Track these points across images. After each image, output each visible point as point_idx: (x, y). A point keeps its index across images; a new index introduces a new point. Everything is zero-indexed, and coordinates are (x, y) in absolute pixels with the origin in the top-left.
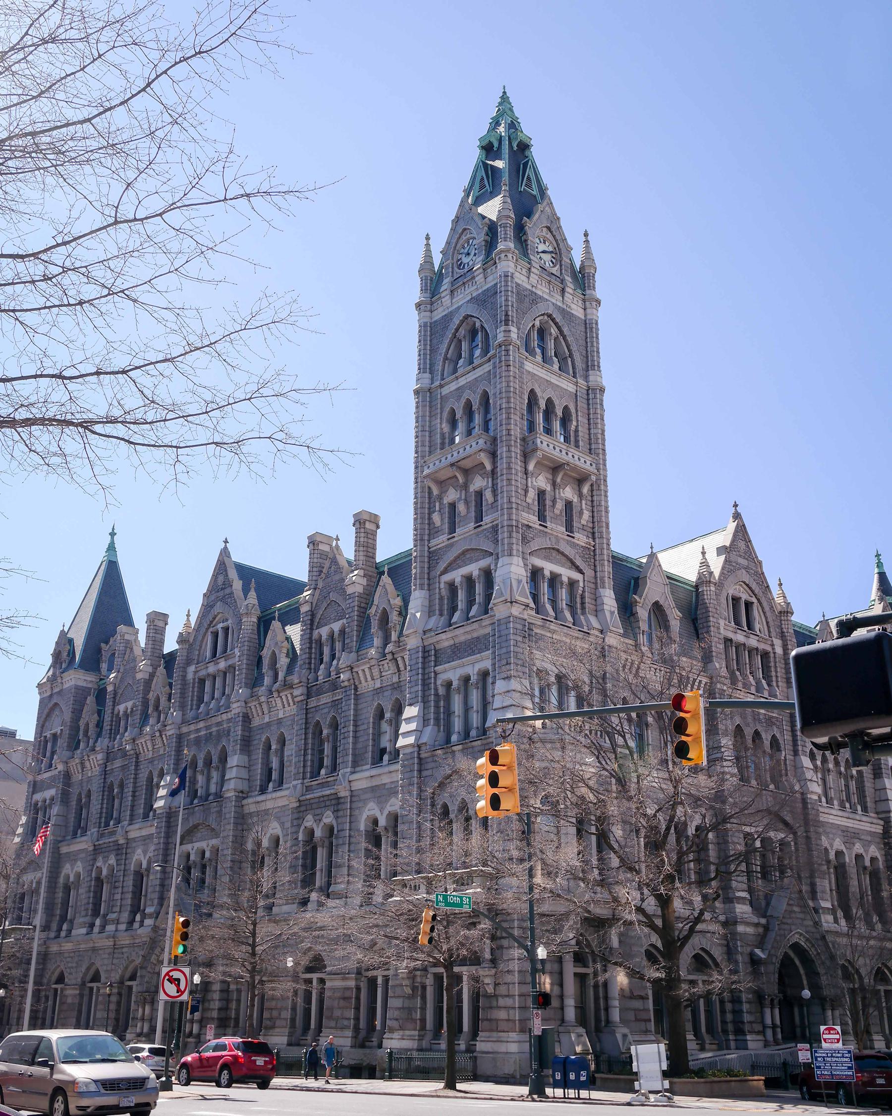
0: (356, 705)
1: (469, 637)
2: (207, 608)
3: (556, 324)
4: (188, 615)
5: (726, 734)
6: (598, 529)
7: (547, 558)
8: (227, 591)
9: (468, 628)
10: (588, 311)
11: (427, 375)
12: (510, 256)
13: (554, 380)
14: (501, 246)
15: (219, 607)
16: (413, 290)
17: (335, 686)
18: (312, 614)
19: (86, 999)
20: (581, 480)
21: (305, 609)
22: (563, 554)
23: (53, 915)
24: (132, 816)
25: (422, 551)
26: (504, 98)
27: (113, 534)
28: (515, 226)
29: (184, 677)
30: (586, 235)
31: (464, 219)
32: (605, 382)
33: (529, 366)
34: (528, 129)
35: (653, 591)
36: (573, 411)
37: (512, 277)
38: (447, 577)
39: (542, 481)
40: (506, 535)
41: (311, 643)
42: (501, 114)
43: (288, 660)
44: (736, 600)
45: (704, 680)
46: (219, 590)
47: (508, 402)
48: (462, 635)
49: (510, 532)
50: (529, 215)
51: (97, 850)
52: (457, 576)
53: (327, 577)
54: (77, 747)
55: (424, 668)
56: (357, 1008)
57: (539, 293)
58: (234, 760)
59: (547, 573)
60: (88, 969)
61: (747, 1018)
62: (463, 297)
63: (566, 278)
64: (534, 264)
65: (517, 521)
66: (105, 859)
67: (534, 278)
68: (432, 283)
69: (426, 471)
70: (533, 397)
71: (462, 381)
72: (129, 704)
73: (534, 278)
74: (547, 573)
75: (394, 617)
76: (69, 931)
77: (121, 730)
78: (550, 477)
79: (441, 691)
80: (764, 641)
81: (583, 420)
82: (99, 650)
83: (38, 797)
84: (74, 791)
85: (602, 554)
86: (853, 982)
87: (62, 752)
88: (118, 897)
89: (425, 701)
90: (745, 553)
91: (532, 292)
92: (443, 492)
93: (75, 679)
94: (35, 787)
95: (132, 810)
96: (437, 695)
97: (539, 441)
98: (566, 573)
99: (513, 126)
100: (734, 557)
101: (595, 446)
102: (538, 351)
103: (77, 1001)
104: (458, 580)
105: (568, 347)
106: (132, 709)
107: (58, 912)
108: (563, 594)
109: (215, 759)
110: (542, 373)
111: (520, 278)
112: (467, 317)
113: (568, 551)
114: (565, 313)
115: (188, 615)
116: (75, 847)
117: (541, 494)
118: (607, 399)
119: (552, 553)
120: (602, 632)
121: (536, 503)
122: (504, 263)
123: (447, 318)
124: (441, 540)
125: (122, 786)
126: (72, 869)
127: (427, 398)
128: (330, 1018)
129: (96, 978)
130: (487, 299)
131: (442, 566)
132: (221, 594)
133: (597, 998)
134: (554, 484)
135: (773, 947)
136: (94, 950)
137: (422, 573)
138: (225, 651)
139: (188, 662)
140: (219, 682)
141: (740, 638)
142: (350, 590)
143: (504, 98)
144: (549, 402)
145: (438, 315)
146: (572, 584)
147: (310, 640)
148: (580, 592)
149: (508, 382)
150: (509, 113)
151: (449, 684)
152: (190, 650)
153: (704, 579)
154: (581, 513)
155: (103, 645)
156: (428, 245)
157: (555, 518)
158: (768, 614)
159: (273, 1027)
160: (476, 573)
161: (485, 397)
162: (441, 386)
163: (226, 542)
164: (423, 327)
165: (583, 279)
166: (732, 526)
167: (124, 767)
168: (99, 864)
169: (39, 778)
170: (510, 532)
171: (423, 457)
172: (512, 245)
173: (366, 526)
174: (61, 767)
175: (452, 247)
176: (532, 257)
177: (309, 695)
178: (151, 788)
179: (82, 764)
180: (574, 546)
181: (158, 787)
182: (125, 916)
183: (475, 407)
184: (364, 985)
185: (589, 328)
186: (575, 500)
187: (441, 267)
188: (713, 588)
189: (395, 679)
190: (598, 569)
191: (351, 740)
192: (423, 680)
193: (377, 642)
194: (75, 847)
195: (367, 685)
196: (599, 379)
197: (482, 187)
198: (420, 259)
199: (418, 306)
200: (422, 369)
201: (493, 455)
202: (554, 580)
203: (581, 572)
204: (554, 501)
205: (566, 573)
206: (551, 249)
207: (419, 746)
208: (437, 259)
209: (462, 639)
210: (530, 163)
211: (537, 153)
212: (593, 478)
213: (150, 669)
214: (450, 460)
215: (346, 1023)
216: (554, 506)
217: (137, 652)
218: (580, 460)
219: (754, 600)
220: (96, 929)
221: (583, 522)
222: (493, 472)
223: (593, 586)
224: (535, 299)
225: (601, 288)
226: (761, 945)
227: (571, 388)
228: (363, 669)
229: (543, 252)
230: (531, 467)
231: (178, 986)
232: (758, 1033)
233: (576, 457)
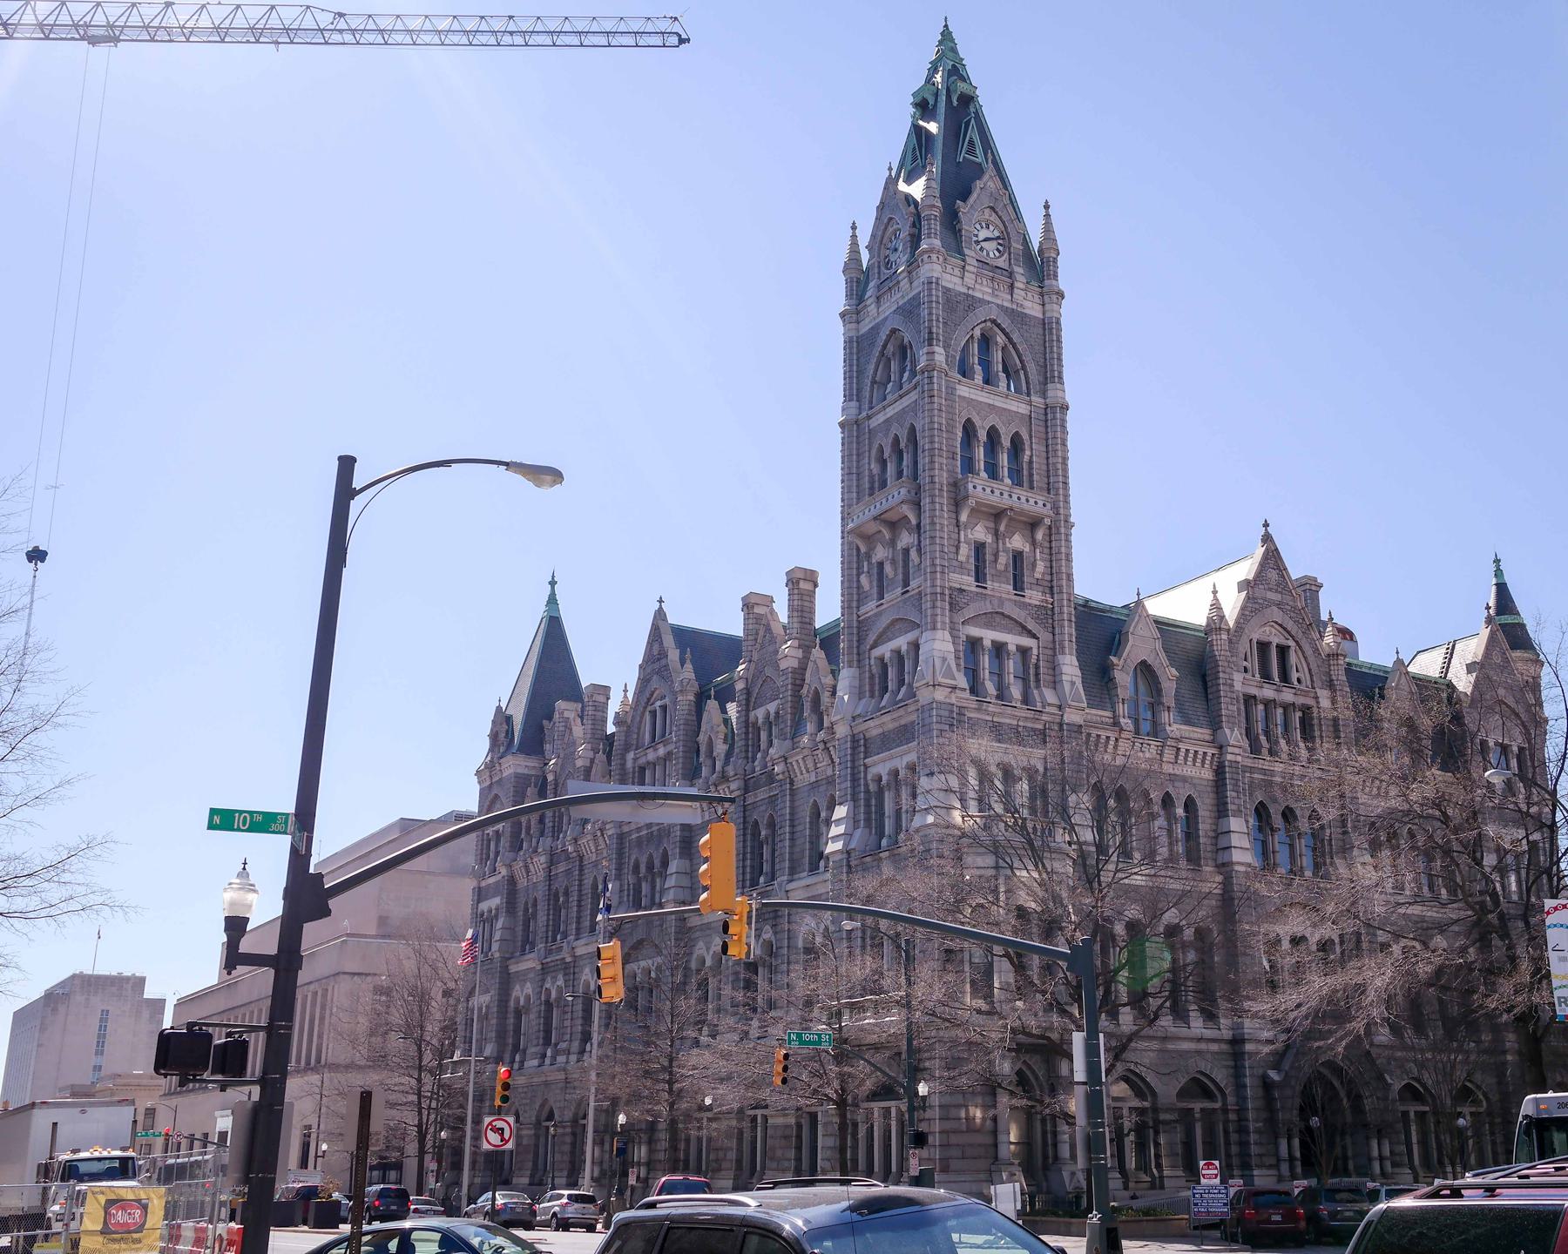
0: (792, 801)
1: (896, 724)
2: (644, 682)
3: (1003, 330)
4: (626, 691)
5: (1238, 813)
6: (1057, 577)
7: (989, 625)
8: (663, 662)
9: (895, 715)
10: (1048, 307)
11: (854, 404)
12: (934, 257)
13: (999, 402)
15: (655, 682)
16: (836, 296)
17: (770, 778)
18: (748, 691)
19: (542, 1140)
20: (1033, 524)
21: (740, 686)
22: (1009, 617)
23: (506, 1045)
24: (578, 929)
25: (850, 621)
26: (946, 35)
27: (553, 583)
28: (943, 215)
29: (623, 765)
30: (1047, 207)
31: (891, 201)
33: (963, 391)
35: (1140, 646)
36: (1025, 436)
38: (876, 652)
39: (980, 533)
40: (929, 605)
41: (747, 727)
43: (726, 747)
44: (1263, 647)
45: (1210, 751)
46: (654, 665)
47: (932, 442)
48: (888, 722)
49: (934, 601)
50: (965, 195)
51: (545, 970)
52: (885, 650)
53: (762, 647)
54: (521, 848)
55: (853, 761)
56: (799, 1148)
57: (978, 295)
58: (673, 867)
59: (987, 643)
60: (542, 1106)
61: (1254, 1150)
62: (889, 306)
63: (1016, 269)
65: (943, 587)
66: (555, 979)
67: (969, 279)
68: (859, 283)
69: (851, 525)
70: (969, 429)
71: (890, 412)
72: (772, 707)
73: (969, 279)
74: (987, 643)
75: (825, 698)
76: (522, 1063)
77: (763, 745)
78: (992, 525)
79: (873, 787)
80: (1305, 694)
81: (1039, 448)
82: (541, 729)
83: (484, 906)
84: (521, 900)
85: (1061, 613)
86: (1424, 1102)
87: (506, 854)
88: (567, 1023)
89: (854, 799)
90: (1278, 585)
91: (968, 295)
92: (871, 549)
93: (515, 765)
94: (480, 895)
95: (578, 923)
96: (867, 791)
97: (970, 486)
98: (1012, 640)
100: (1259, 592)
101: (1055, 483)
102: (978, 368)
103: (532, 1142)
104: (888, 656)
105: (1020, 357)
106: (777, 713)
107: (510, 1041)
108: (1011, 666)
109: (657, 863)
110: (983, 397)
111: (951, 281)
113: (1017, 613)
114: (1018, 317)
115: (626, 691)
116: (523, 966)
117: (979, 548)
119: (994, 618)
120: (1060, 707)
121: (972, 560)
122: (927, 267)
123: (875, 330)
124: (870, 607)
125: (567, 893)
126: (708, 949)
127: (855, 431)
128: (772, 1159)
129: (550, 1117)
130: (910, 311)
131: (871, 638)
132: (656, 666)
133: (1044, 1133)
134: (996, 534)
135: (1292, 1067)
136: (546, 1084)
137: (850, 647)
138: (664, 735)
139: (627, 749)
141: (1268, 692)
142: (783, 665)
143: (946, 35)
144: (993, 434)
145: (865, 327)
146: (1024, 652)
147: (746, 722)
148: (1034, 661)
149: (932, 417)
150: (950, 54)
152: (628, 733)
153: (1216, 623)
154: (1034, 565)
155: (545, 722)
156: (1047, 216)
157: (998, 576)
158: (1311, 659)
159: (720, 1170)
160: (904, 648)
162: (869, 417)
164: (849, 342)
165: (1040, 267)
166: (1260, 551)
167: (568, 872)
168: (548, 985)
169: (483, 884)
170: (934, 601)
171: (850, 506)
172: (937, 243)
173: (802, 584)
174: (504, 871)
175: (880, 240)
176: (967, 251)
177: (746, 790)
178: (819, 822)
179: (526, 867)
180: (1024, 606)
181: (828, 823)
182: (576, 1045)
183: (902, 445)
184: (805, 1122)
185: (1049, 330)
186: (1027, 549)
188: (1224, 637)
189: (829, 772)
190: (1057, 631)
191: (787, 843)
192: (853, 775)
193: (810, 727)
194: (523, 966)
195: (804, 779)
196: (1060, 394)
197: (914, 160)
198: (843, 256)
199: (843, 315)
200: (848, 397)
201: (917, 505)
202: (999, 649)
203: (1034, 636)
204: (996, 555)
205: (1012, 640)
206: (997, 234)
207: (848, 853)
208: (865, 257)
209: (891, 726)
212: (1047, 521)
213: (800, 653)
214: (874, 512)
215: (786, 1164)
216: (996, 561)
217: (777, 630)
218: (1031, 502)
219: (1291, 643)
220: (547, 1061)
221: (1038, 575)
222: (919, 525)
223: (1050, 652)
224: (972, 303)
225: (1067, 276)
226: (1277, 1066)
227: (1023, 409)
228: (796, 759)
229: (986, 240)
230: (964, 517)
231: (502, 1135)
232: (1270, 1167)
233: (1023, 499)
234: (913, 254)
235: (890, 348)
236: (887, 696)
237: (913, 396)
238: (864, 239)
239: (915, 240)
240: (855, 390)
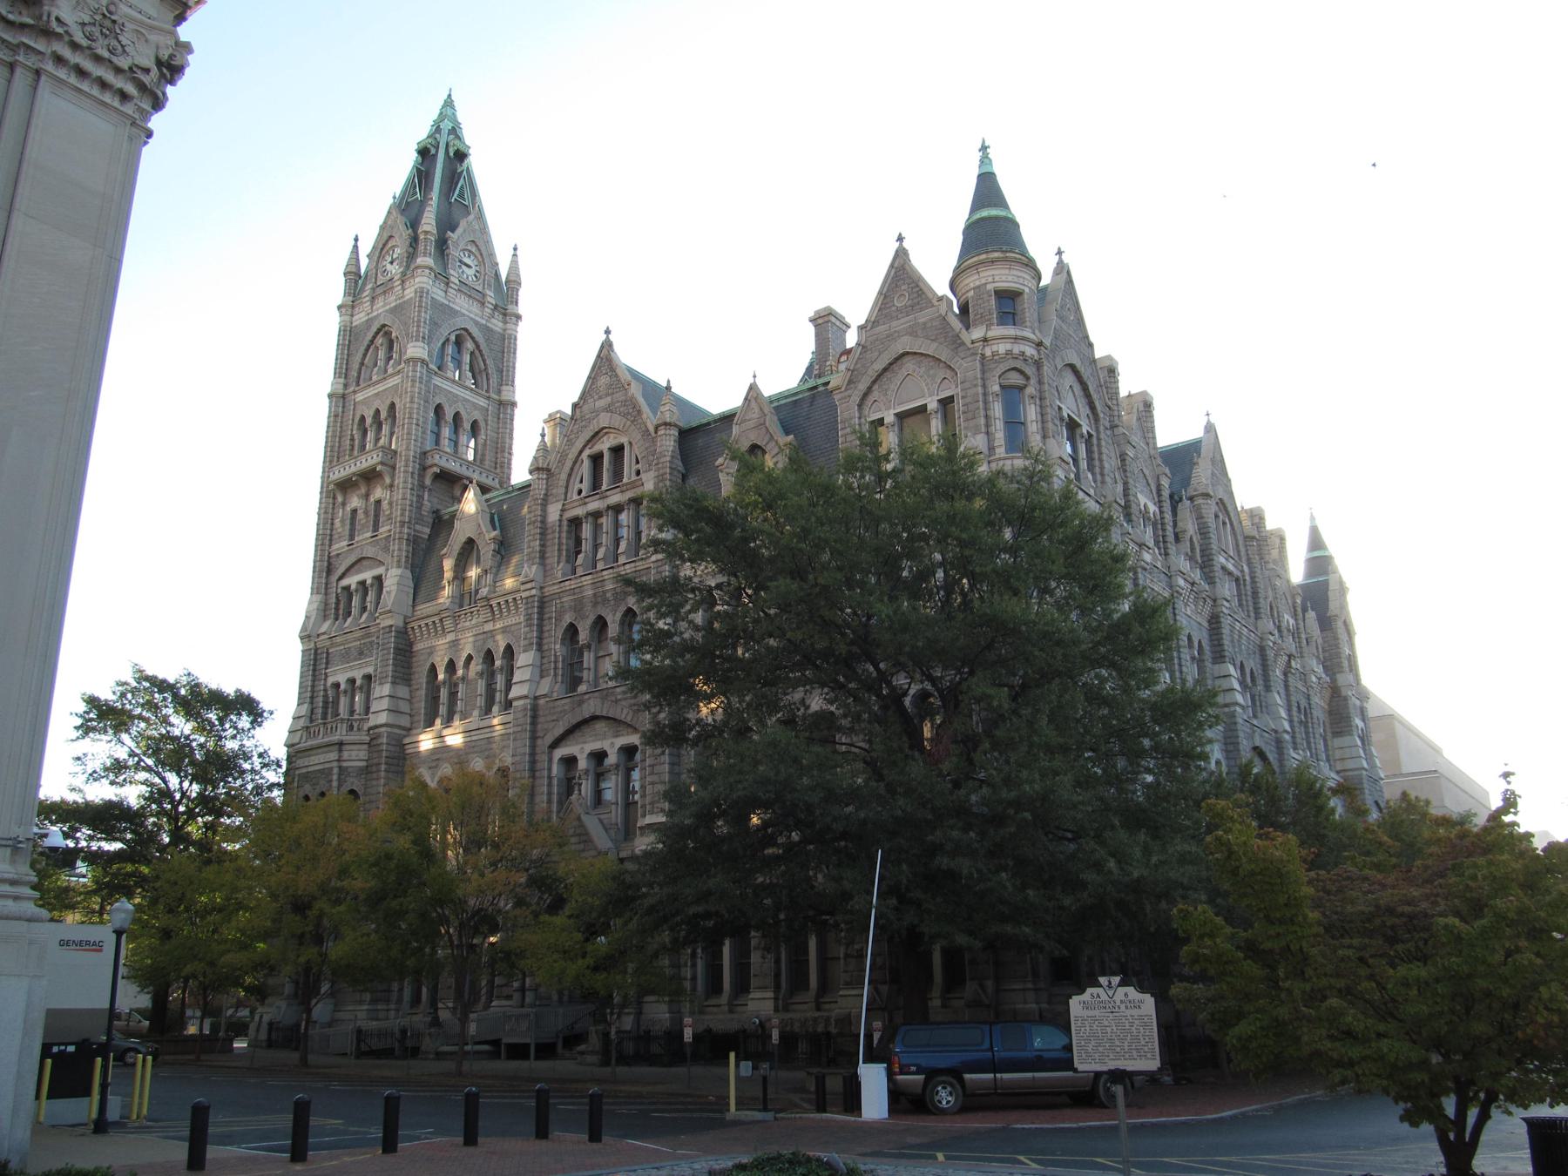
14: (420, 261)
32: (518, 397)
34: (471, 137)
38: (345, 582)
62: (381, 307)
99: (455, 131)
127: (339, 399)
140: (606, 522)
144: (457, 416)
151: (337, 685)
161: (393, 406)
163: (608, 332)
187: (366, 273)
208: (364, 263)
211: (478, 164)
235: (379, 340)
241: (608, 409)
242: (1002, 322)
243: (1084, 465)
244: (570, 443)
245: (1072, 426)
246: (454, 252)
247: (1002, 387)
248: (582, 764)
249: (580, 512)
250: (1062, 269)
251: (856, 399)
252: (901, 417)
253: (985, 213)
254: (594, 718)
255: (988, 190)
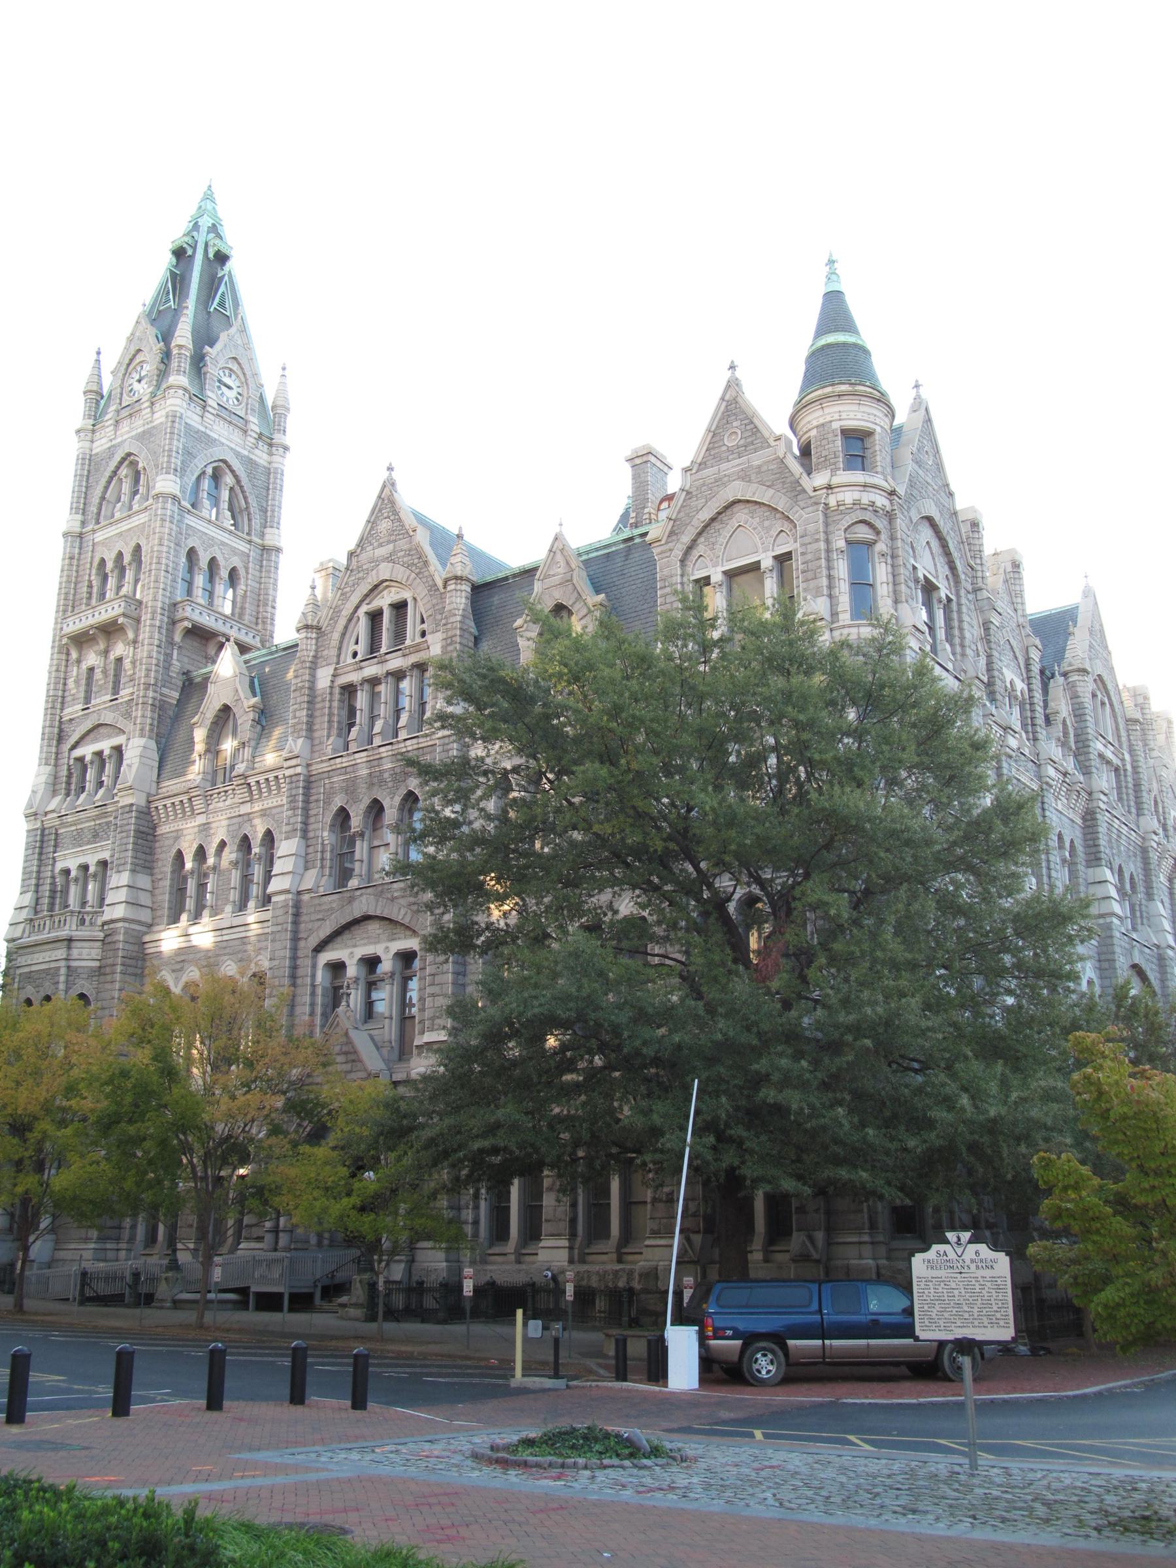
28: (192, 357)
34: (234, 241)
36: (242, 572)
37: (181, 418)
38: (78, 753)
42: (201, 211)
52: (87, 751)
64: (210, 402)
70: (192, 554)
105: (245, 498)
112: (129, 454)
118: (284, 560)
144: (213, 562)
151: (67, 872)
156: (98, 361)
165: (270, 426)
210: (226, 278)
234: (158, 387)
235: (123, 471)
236: (83, 796)
237: (142, 518)
238: (110, 363)
239: (163, 374)
240: (81, 506)
241: (390, 559)
242: (849, 467)
243: (941, 634)
244: (345, 597)
245: (929, 588)
246: (212, 370)
247: (849, 542)
248: (352, 971)
249: (354, 677)
250: (920, 406)
251: (678, 553)
252: (731, 575)
253: (831, 339)
254: (367, 918)
255: (834, 312)
